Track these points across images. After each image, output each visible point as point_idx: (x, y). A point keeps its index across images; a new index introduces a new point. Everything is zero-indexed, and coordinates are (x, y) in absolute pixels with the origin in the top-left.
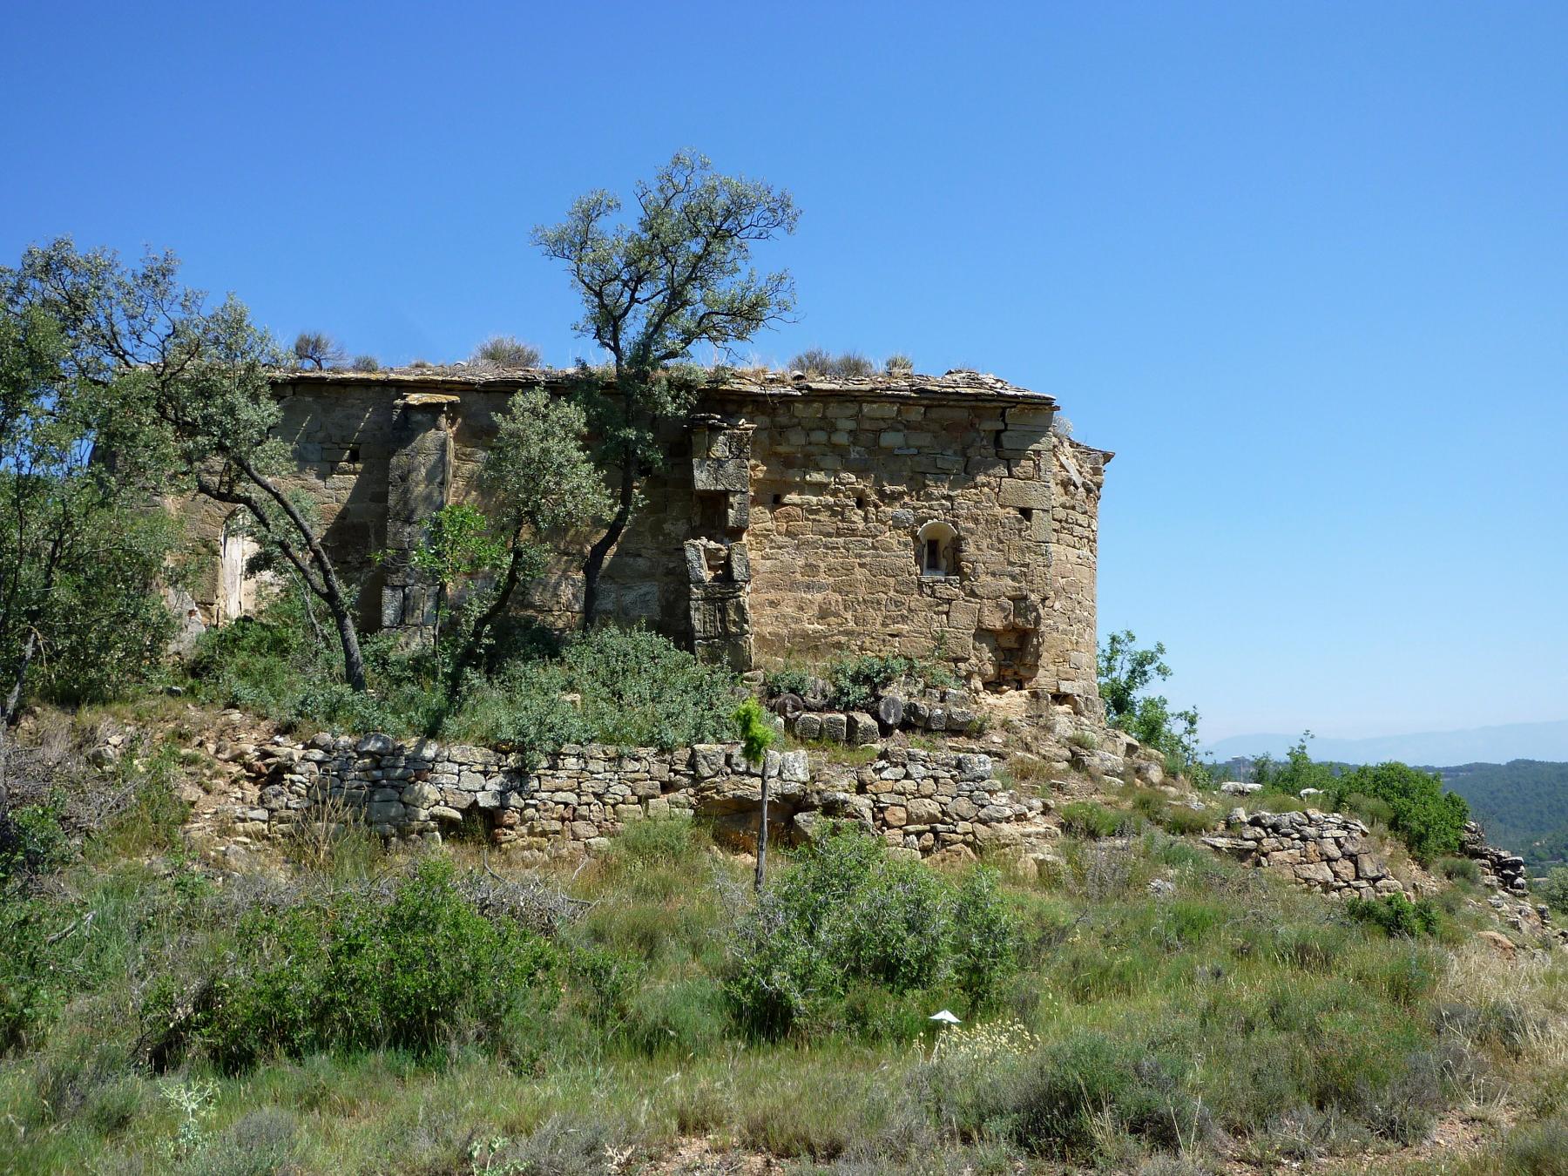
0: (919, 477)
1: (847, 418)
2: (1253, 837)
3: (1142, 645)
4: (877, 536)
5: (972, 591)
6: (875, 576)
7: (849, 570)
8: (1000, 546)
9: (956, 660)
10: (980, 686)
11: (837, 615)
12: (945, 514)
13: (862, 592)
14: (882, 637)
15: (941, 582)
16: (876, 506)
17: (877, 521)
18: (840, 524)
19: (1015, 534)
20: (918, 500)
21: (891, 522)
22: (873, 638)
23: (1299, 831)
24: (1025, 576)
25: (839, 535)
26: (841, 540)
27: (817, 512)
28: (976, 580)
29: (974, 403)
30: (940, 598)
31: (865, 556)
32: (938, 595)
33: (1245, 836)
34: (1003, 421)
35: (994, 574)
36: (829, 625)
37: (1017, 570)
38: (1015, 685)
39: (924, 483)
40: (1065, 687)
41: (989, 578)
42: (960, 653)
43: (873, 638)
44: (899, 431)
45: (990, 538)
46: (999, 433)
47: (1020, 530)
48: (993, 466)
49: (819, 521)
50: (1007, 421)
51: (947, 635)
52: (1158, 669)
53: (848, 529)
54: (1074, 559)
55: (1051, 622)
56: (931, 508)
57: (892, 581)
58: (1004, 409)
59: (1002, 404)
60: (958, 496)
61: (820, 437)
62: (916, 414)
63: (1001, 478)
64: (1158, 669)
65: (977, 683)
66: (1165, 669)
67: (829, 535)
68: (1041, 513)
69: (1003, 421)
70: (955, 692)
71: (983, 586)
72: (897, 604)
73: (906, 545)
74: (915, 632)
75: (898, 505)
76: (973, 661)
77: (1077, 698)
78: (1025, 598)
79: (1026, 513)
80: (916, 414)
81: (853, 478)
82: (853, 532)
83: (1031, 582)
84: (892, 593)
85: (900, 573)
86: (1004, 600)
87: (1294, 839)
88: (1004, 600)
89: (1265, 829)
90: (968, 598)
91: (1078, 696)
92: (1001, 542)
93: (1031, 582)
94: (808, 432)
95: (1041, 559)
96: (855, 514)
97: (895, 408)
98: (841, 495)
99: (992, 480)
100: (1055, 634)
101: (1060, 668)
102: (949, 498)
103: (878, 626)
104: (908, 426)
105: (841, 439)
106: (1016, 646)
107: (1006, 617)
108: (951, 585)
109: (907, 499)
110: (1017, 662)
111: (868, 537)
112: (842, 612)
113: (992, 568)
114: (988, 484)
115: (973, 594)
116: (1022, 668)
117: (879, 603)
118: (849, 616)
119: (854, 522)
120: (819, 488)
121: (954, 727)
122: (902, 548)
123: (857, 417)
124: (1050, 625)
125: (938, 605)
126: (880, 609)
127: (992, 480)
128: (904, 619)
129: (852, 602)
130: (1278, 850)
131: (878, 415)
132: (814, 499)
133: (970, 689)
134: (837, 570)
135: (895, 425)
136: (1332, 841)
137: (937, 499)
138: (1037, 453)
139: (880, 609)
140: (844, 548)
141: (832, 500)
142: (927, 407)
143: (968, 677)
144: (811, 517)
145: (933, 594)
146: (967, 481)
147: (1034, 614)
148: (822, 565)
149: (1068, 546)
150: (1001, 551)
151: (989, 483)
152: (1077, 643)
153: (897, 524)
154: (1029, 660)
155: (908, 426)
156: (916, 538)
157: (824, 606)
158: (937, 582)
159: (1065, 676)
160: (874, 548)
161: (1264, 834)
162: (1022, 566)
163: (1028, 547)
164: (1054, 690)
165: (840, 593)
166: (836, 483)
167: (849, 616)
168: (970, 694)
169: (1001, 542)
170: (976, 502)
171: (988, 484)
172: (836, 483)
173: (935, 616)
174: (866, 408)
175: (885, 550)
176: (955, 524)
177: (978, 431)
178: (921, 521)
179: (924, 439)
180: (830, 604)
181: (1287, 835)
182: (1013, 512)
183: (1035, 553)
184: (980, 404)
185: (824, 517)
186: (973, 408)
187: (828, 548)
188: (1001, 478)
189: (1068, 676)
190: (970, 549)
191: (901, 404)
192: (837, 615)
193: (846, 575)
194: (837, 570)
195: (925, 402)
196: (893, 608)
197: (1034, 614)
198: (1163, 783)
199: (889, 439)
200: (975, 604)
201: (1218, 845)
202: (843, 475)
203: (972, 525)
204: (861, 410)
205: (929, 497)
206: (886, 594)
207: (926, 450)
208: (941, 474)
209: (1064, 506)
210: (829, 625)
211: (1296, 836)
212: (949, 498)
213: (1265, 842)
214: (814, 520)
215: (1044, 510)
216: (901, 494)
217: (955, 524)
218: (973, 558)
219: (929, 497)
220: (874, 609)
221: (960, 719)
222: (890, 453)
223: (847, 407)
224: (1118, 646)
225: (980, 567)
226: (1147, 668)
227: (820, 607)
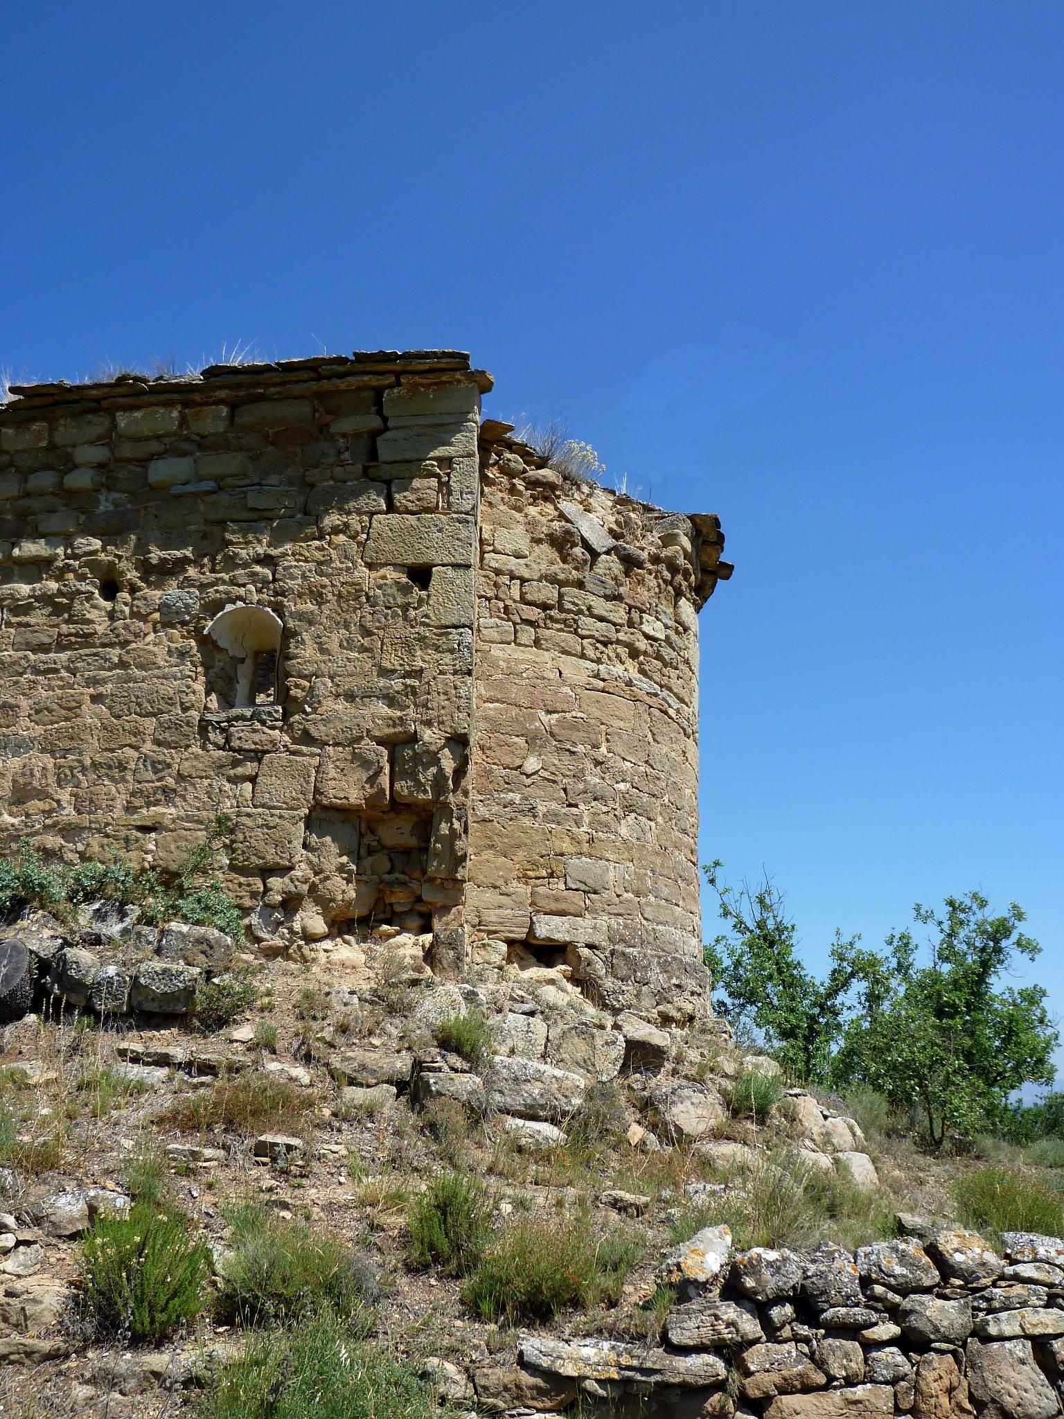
0: (216, 530)
1: (92, 443)
2: (706, 1335)
3: (996, 911)
4: (128, 642)
5: (306, 732)
6: (118, 717)
7: (72, 710)
8: (366, 642)
9: (267, 872)
10: (318, 925)
11: (43, 795)
12: (259, 591)
13: (92, 749)
14: (123, 834)
15: (242, 718)
16: (133, 590)
17: (134, 615)
18: (65, 628)
19: (395, 615)
20: (213, 571)
21: (157, 616)
22: (107, 836)
23: (896, 1314)
24: (414, 693)
25: (61, 648)
26: (64, 656)
27: (27, 609)
28: (315, 710)
29: (314, 386)
30: (240, 750)
31: (104, 682)
32: (235, 743)
33: (675, 1337)
34: (379, 412)
35: (350, 697)
36: (28, 815)
37: (397, 684)
38: (416, 922)
39: (223, 538)
40: (550, 928)
41: (341, 705)
42: (271, 856)
43: (107, 836)
44: (184, 454)
45: (347, 627)
46: (374, 435)
47: (405, 608)
48: (356, 494)
49: (27, 625)
50: (386, 412)
51: (244, 820)
52: (1019, 944)
53: (77, 635)
54: (582, 679)
55: (517, 797)
56: (233, 582)
57: (150, 724)
58: (379, 392)
59: (374, 381)
60: (284, 555)
61: (44, 480)
62: (213, 421)
63: (372, 514)
64: (1019, 944)
65: (311, 919)
66: (1029, 942)
67: (42, 648)
68: (450, 572)
69: (379, 412)
70: (185, 928)
71: (325, 722)
72: (158, 767)
73: (182, 654)
74: (188, 819)
75: (175, 584)
76: (302, 871)
77: (585, 952)
78: (414, 738)
79: (420, 575)
80: (213, 421)
81: (97, 544)
82: (86, 639)
83: (425, 706)
84: (148, 747)
85: (164, 707)
86: (368, 745)
87: (880, 1345)
88: (368, 745)
89: (761, 1310)
90: (294, 747)
91: (591, 946)
92: (367, 633)
93: (425, 706)
94: (25, 474)
95: (447, 658)
96: (95, 607)
97: (175, 414)
98: (71, 576)
99: (354, 521)
100: (527, 821)
101: (541, 890)
102: (267, 561)
103: (118, 812)
104: (204, 444)
105: (81, 480)
106: (412, 842)
107: (372, 780)
108: (263, 723)
109: (192, 572)
110: (417, 874)
111: (111, 645)
112: (53, 789)
113: (347, 684)
114: (344, 529)
115: (307, 738)
116: (425, 886)
117: (122, 767)
118: (65, 795)
119: (90, 622)
120: (36, 568)
121: (150, 1007)
122: (173, 660)
123: (109, 438)
124: (512, 803)
125: (235, 764)
126: (124, 780)
127: (354, 521)
128: (168, 795)
129: (72, 768)
130: (807, 1389)
131: (146, 430)
132: (24, 589)
133: (291, 931)
134: (50, 711)
135: (173, 446)
136: (1022, 1349)
137: (246, 565)
138: (447, 462)
139: (124, 780)
140: (68, 669)
141: (53, 586)
142: (234, 406)
143: (290, 904)
144: (14, 620)
145: (226, 746)
146: (302, 525)
147: (433, 770)
148: (24, 703)
149: (564, 652)
150: (367, 650)
151: (346, 525)
152: (591, 840)
153: (169, 617)
154: (435, 867)
155: (204, 444)
156: (206, 643)
157: (21, 781)
158: (237, 718)
159: (554, 906)
160: (123, 665)
161: (750, 1326)
162: (408, 675)
163: (421, 639)
164: (521, 934)
165: (52, 753)
166: (67, 557)
167: (65, 795)
168: (292, 942)
169: (367, 633)
170: (320, 563)
171: (344, 529)
172: (67, 557)
173: (227, 786)
174: (122, 420)
175: (141, 667)
176: (279, 609)
177: (331, 438)
178: (213, 607)
179: (230, 463)
180: (32, 775)
181: (850, 1330)
182: (391, 574)
183: (437, 649)
184: (325, 384)
185: (37, 618)
186: (321, 396)
187: (37, 672)
188: (372, 514)
189: (563, 906)
190: (306, 653)
191: (185, 405)
192: (43, 795)
193: (67, 719)
194: (50, 711)
195: (222, 394)
196: (150, 775)
197: (433, 770)
198: (718, 1135)
199: (161, 471)
200: (309, 759)
201: (569, 1370)
202: (80, 541)
203: (310, 606)
204: (114, 426)
205: (231, 563)
206: (137, 748)
207: (229, 481)
208: (255, 520)
209: (553, 580)
210: (28, 815)
211: (887, 1330)
212: (267, 561)
213: (754, 1358)
214: (20, 624)
215: (456, 566)
216: (182, 563)
217: (279, 609)
218: (311, 669)
219: (231, 563)
220: (112, 779)
221: (158, 987)
222: (160, 492)
223: (89, 422)
224: (962, 916)
225: (324, 686)
226: (1004, 943)
227: (14, 781)
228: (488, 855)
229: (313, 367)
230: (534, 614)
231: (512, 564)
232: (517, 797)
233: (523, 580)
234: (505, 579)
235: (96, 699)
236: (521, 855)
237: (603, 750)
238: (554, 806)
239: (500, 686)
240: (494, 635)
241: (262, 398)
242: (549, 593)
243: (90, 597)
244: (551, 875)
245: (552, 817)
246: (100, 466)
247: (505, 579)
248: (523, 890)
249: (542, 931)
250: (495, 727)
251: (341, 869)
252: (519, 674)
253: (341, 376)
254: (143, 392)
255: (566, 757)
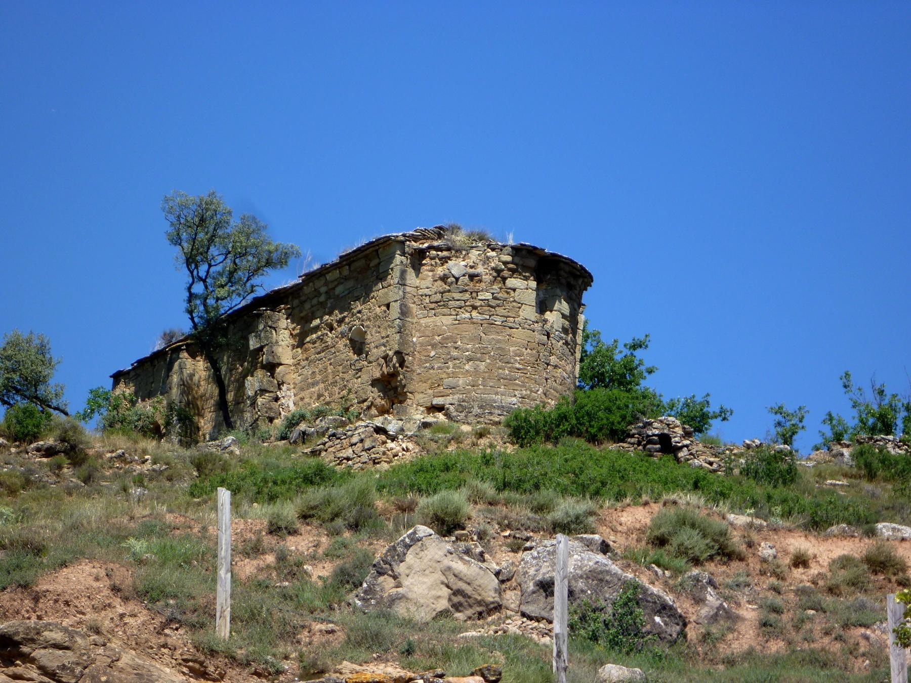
25: (323, 352)
40: (438, 401)
44: (342, 283)
54: (450, 322)
67: (319, 353)
100: (431, 371)
107: (381, 369)
118: (326, 394)
142: (349, 265)
149: (444, 315)
153: (343, 335)
155: (346, 279)
163: (389, 326)
164: (429, 405)
167: (326, 394)
179: (350, 284)
191: (339, 268)
195: (344, 263)
228: (420, 384)
229: (359, 250)
230: (433, 306)
231: (427, 291)
232: (428, 365)
233: (430, 296)
234: (424, 297)
235: (331, 364)
236: (430, 381)
237: (459, 343)
238: (439, 365)
239: (423, 332)
240: (421, 316)
241: (354, 261)
242: (439, 297)
243: (327, 334)
244: (439, 385)
245: (439, 368)
246: (326, 292)
247: (424, 297)
248: (430, 391)
249: (434, 403)
250: (422, 345)
251: (379, 396)
252: (429, 327)
253: (366, 250)
254: (329, 268)
255: (444, 349)
